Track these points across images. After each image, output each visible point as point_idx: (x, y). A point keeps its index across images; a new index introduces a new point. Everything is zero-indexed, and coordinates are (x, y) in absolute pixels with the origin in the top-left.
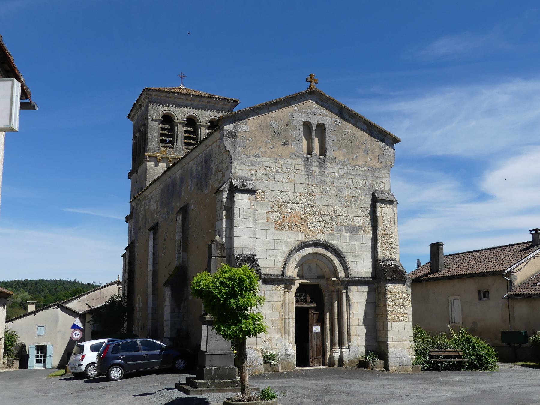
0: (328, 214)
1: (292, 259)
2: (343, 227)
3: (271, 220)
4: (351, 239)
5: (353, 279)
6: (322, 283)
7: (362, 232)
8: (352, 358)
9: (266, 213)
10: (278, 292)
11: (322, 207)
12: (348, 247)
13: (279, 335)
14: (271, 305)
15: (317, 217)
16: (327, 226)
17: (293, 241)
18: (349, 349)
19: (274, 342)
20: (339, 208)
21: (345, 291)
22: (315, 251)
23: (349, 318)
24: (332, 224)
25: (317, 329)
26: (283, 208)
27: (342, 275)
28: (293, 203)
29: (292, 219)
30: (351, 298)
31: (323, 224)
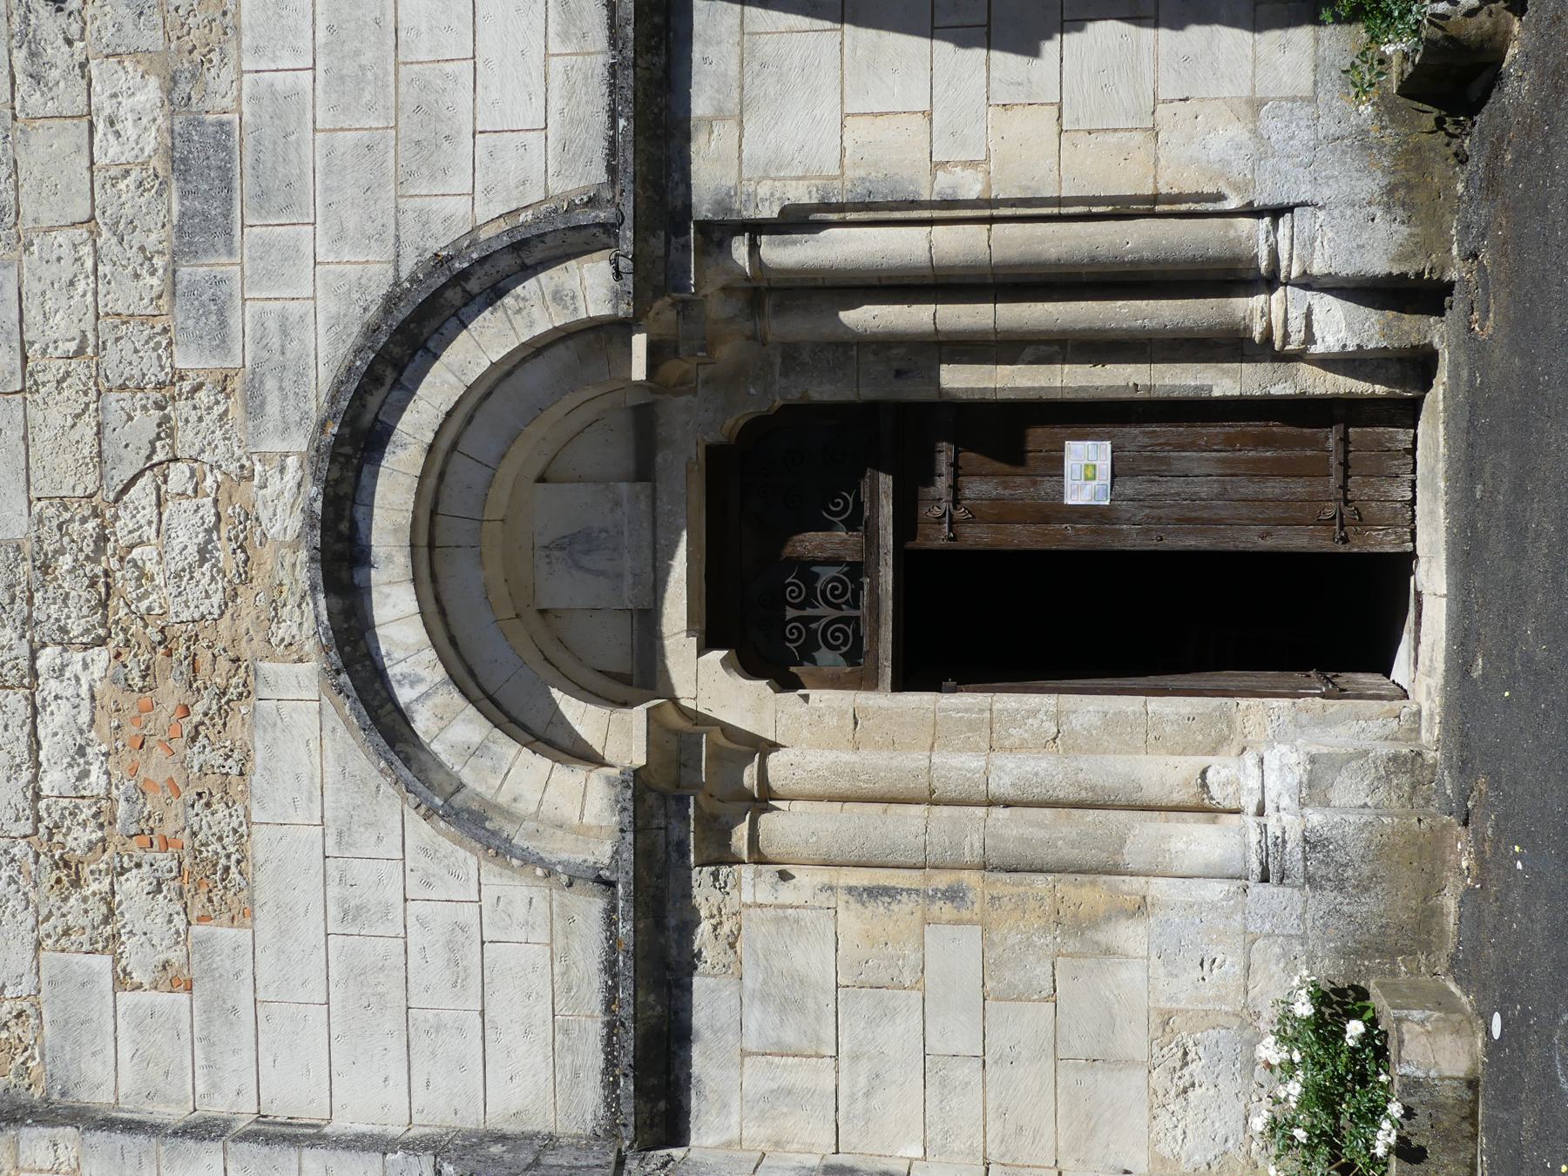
0: (89, 419)
1: (479, 781)
2: (184, 272)
3: (176, 956)
4: (280, 199)
5: (626, 182)
6: (694, 426)
7: (219, 79)
8: (1370, 185)
9: (125, 998)
10: (756, 931)
11: (42, 486)
12: (352, 221)
13: (1130, 936)
14: (866, 999)
15: (122, 531)
16: (187, 441)
17: (331, 769)
18: (1276, 213)
19: (1181, 989)
20: (33, 314)
21: (740, 250)
22: (402, 560)
23: (987, 211)
24: (169, 387)
25: (1086, 470)
26: (80, 837)
27: (589, 287)
28: (35, 744)
29: (158, 766)
30: (800, 194)
31: (178, 475)
